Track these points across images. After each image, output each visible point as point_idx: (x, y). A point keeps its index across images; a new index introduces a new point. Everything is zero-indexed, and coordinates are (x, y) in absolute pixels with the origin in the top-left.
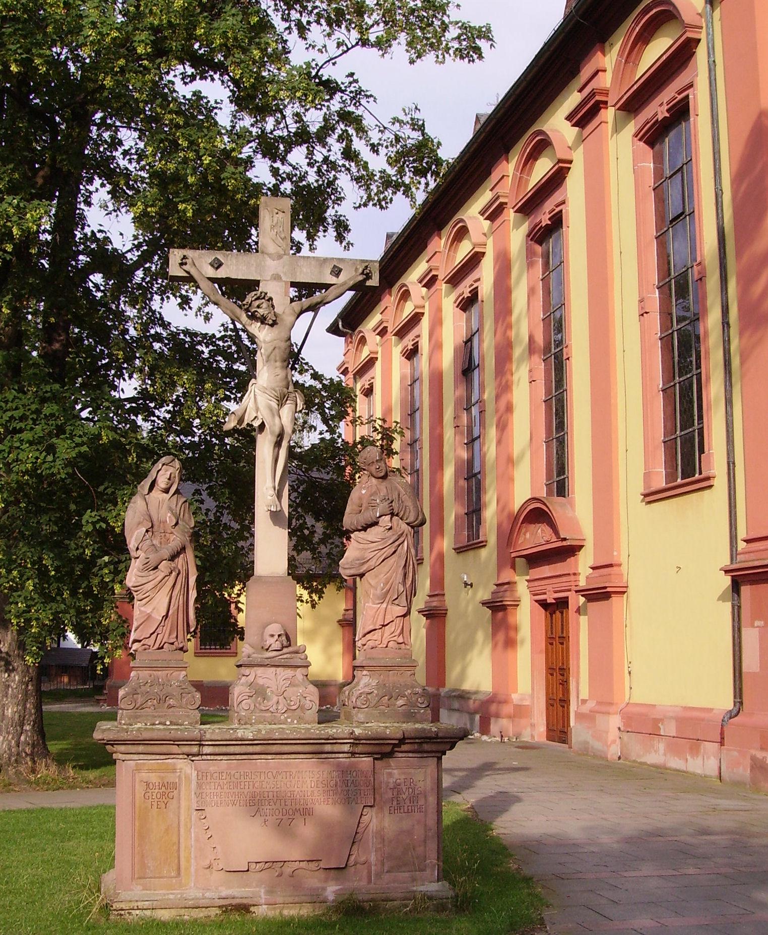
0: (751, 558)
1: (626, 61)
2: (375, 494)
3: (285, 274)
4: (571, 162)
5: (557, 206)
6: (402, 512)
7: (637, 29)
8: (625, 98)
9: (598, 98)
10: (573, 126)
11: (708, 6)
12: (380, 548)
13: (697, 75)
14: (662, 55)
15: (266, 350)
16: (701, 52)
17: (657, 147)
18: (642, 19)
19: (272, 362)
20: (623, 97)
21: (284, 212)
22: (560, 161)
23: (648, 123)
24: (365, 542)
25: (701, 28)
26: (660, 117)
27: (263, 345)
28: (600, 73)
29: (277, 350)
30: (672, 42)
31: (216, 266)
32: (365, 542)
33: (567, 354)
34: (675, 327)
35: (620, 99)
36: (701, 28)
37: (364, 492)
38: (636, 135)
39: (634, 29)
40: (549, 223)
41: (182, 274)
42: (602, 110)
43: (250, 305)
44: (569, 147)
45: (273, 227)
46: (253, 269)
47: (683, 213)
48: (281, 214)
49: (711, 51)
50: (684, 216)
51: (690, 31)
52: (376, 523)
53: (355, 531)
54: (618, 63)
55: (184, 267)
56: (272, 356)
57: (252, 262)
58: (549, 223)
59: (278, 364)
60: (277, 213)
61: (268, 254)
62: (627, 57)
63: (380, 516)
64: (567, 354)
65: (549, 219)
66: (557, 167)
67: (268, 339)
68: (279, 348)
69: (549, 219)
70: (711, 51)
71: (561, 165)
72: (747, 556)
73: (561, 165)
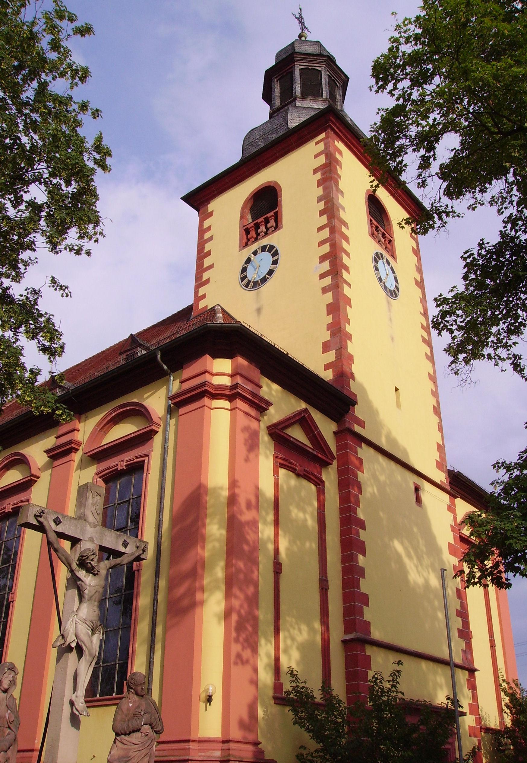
0: (164, 754)
1: (100, 430)
2: (138, 707)
3: (97, 539)
4: (38, 477)
5: (20, 502)
6: (155, 723)
7: (113, 414)
8: (96, 451)
9: (73, 445)
10: (48, 457)
11: (169, 416)
12: (141, 749)
13: (152, 451)
14: (131, 434)
15: (90, 591)
16: (158, 440)
17: (110, 484)
18: (118, 410)
19: (93, 602)
20: (95, 449)
21: (100, 496)
22: (32, 475)
23: (109, 469)
24: (129, 744)
25: (160, 426)
26: (119, 468)
27: (88, 588)
28: (75, 431)
29: (97, 594)
30: (137, 430)
31: (58, 523)
32: (129, 744)
33: (12, 598)
34: (108, 596)
35: (92, 450)
36: (160, 426)
37: (131, 705)
38: (97, 474)
39: (112, 414)
40: (11, 511)
41: (35, 523)
42: (73, 453)
43: (88, 558)
44: (39, 468)
45: (94, 504)
46: (79, 530)
47: (126, 527)
48: (98, 497)
49: (165, 440)
50: (126, 529)
51: (155, 426)
52: (139, 730)
53: (122, 734)
54: (94, 430)
55: (39, 519)
56: (94, 598)
57: (79, 526)
58: (11, 511)
59: (96, 603)
60: (97, 496)
61: (88, 522)
62: (102, 428)
63: (144, 725)
64: (12, 598)
65: (12, 509)
66: (29, 478)
67: (93, 583)
68: (99, 592)
69: (12, 509)
70: (165, 440)
71: (32, 478)
72: (161, 752)
73: (32, 478)
